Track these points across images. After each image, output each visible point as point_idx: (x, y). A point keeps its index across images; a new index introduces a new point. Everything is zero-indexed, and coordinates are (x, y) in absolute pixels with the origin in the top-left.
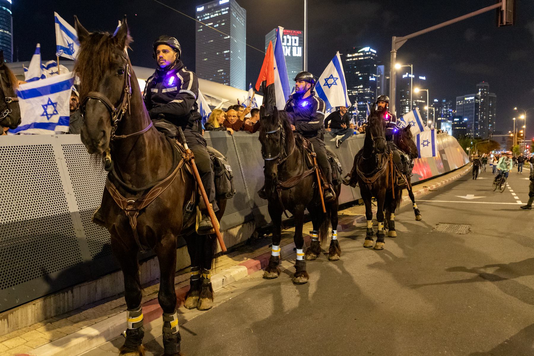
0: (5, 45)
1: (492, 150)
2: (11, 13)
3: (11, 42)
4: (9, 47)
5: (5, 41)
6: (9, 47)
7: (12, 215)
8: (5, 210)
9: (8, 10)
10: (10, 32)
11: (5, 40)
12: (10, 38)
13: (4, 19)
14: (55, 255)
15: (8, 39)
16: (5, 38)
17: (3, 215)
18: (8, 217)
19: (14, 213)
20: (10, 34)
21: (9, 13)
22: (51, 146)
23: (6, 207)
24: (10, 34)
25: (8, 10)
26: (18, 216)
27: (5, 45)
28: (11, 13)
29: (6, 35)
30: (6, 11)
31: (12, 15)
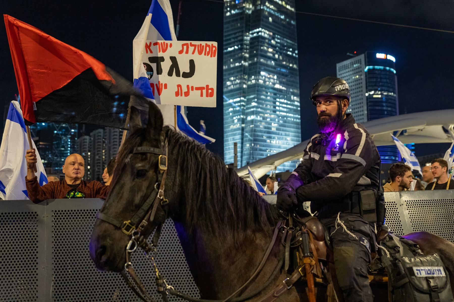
0: (389, 109)
1: (301, 102)
2: (395, 72)
3: (395, 104)
4: (394, 110)
5: (389, 104)
6: (394, 110)
7: (78, 262)
8: (170, 263)
9: (392, 70)
10: (394, 93)
11: (390, 103)
12: (395, 100)
13: (388, 81)
14: (170, 230)
15: (392, 101)
16: (390, 101)
17: (96, 273)
18: (171, 261)
19: (76, 258)
20: (395, 95)
21: (393, 72)
22: (67, 212)
23: (79, 274)
24: (395, 95)
25: (392, 70)
26: (72, 254)
27: (389, 109)
28: (395, 72)
29: (390, 97)
30: (390, 71)
31: (396, 74)
